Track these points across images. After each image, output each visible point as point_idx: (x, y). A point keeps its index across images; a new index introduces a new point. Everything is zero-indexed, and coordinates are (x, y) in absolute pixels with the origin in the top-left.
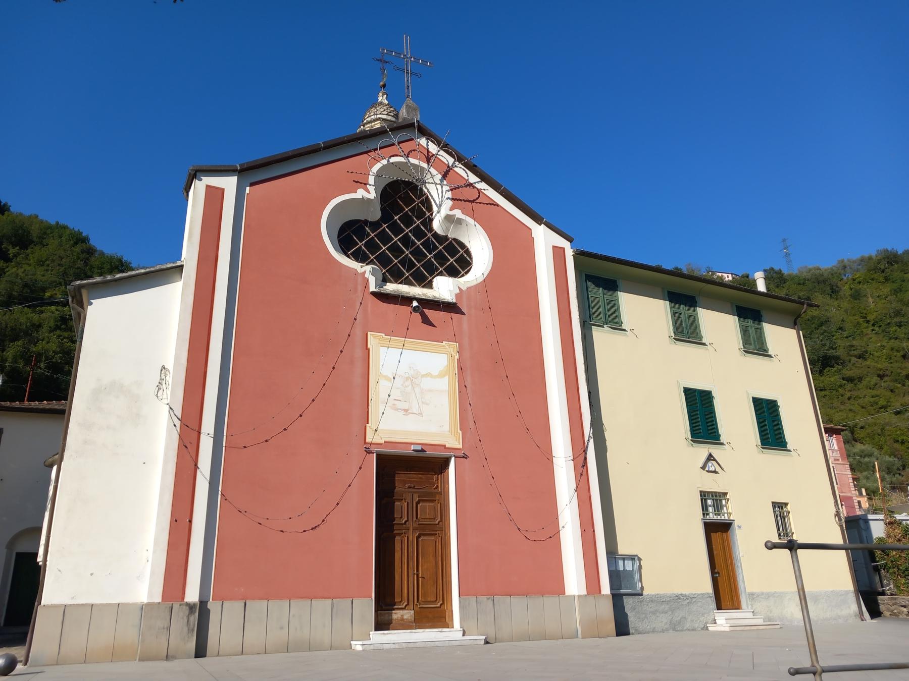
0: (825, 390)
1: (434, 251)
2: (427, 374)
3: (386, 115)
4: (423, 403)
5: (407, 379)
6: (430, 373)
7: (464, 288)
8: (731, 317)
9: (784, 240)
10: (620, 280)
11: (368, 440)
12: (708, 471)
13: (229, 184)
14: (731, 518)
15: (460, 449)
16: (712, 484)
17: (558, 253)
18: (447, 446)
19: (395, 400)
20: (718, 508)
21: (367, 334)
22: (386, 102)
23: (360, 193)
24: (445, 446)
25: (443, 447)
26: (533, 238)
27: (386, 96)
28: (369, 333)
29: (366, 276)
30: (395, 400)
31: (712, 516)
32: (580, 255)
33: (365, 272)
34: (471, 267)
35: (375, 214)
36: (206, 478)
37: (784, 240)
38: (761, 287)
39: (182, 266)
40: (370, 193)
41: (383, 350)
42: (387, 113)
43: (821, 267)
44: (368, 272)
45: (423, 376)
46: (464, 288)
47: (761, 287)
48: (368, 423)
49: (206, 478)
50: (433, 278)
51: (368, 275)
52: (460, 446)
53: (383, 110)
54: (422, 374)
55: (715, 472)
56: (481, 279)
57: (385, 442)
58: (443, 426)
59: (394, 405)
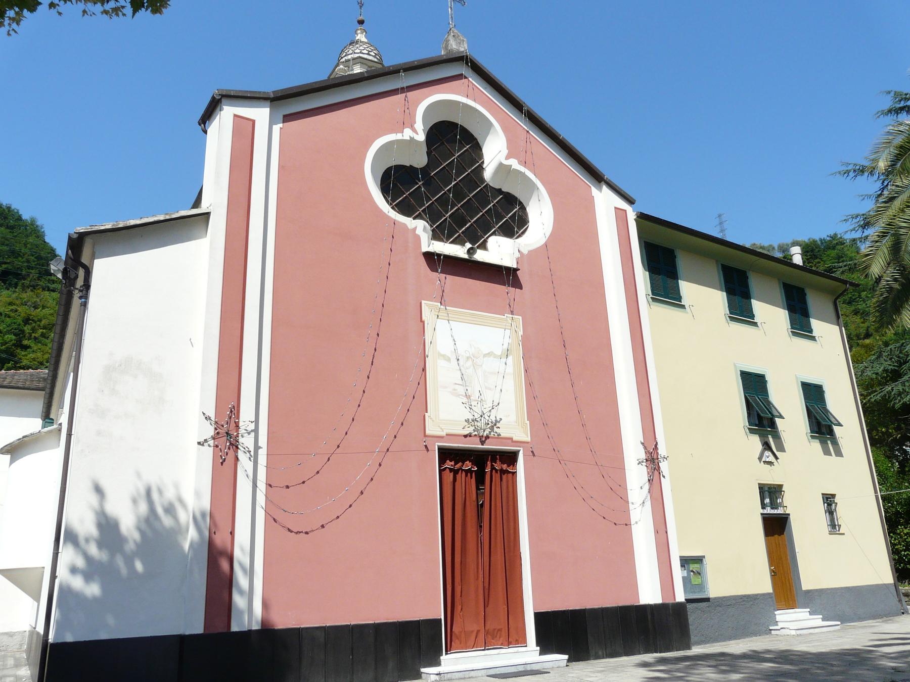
0: (12, 341)
1: (490, 209)
2: (489, 353)
3: (373, 56)
4: (486, 388)
5: (468, 358)
6: (492, 352)
7: (525, 252)
8: (720, 292)
9: (720, 216)
10: (677, 250)
11: (428, 432)
12: (765, 462)
13: (260, 114)
14: (787, 512)
15: (528, 443)
16: (771, 477)
17: (620, 215)
18: (515, 439)
19: (456, 384)
20: (774, 505)
21: (421, 303)
22: (364, 39)
23: (407, 134)
24: (511, 439)
25: (511, 441)
26: (593, 197)
27: (364, 33)
28: (423, 302)
29: (417, 232)
30: (456, 384)
31: (768, 510)
32: (643, 218)
33: (415, 228)
34: (528, 226)
35: (420, 160)
36: (260, 490)
37: (720, 216)
38: (798, 260)
39: (207, 215)
40: (418, 134)
41: (441, 324)
42: (367, 52)
43: (757, 243)
44: (420, 227)
45: (485, 356)
46: (525, 252)
47: (798, 260)
48: (427, 412)
49: (260, 490)
50: (487, 238)
51: (420, 231)
52: (528, 439)
53: (364, 48)
54: (484, 353)
55: (770, 463)
56: (542, 241)
57: (446, 434)
58: (509, 415)
59: (455, 390)
